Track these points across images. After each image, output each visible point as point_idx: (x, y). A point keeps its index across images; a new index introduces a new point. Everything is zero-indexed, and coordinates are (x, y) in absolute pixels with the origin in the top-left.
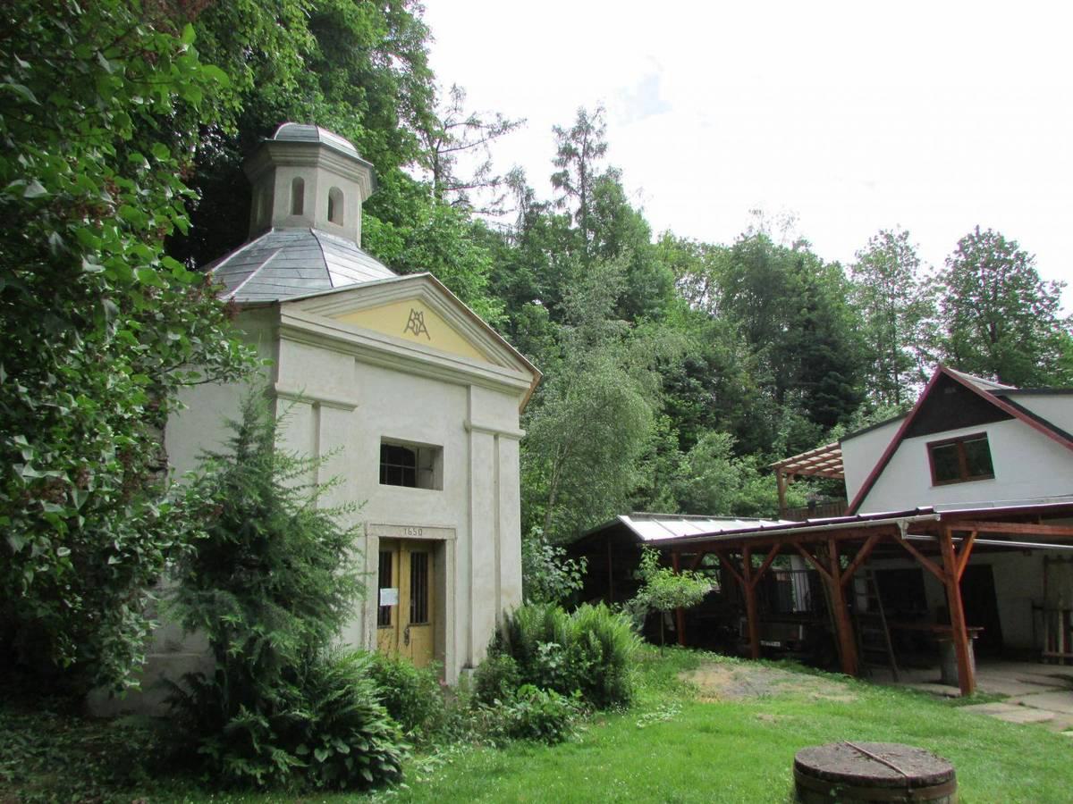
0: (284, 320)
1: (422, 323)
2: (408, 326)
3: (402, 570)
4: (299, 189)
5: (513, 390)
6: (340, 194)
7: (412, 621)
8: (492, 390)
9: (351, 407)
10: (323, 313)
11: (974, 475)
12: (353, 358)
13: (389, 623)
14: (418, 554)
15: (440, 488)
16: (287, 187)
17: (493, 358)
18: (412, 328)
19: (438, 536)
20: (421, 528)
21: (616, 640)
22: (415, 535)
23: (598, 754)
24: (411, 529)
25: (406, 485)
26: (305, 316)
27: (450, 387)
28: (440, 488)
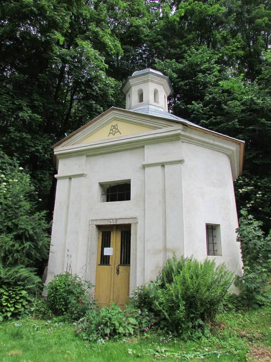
1: (117, 129)
2: (110, 133)
3: (116, 239)
5: (172, 138)
7: (121, 263)
8: (161, 142)
10: (71, 144)
11: (212, 226)
12: (85, 156)
14: (125, 232)
18: (112, 133)
19: (126, 222)
20: (116, 219)
22: (119, 222)
24: (111, 220)
25: (111, 201)
27: (135, 150)
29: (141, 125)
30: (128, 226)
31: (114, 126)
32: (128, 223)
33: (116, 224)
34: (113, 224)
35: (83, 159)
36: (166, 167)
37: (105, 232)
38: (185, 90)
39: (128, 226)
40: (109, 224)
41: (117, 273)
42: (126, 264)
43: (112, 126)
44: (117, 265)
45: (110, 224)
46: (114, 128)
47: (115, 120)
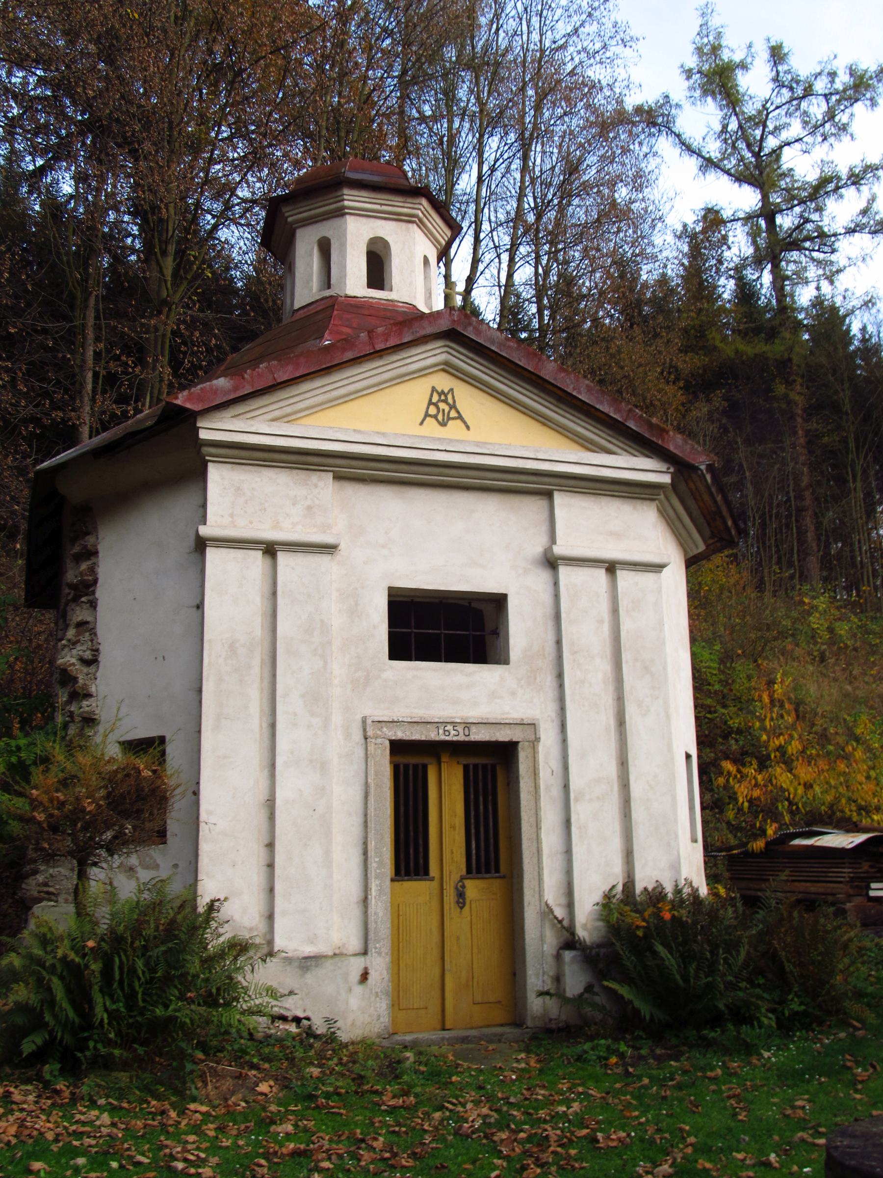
0: (203, 435)
1: (453, 407)
2: (427, 415)
4: (325, 247)
6: (385, 244)
7: (469, 870)
9: (329, 549)
12: (331, 475)
13: (426, 872)
15: (506, 662)
16: (311, 255)
17: (592, 442)
18: (435, 417)
19: (503, 736)
20: (467, 725)
21: (211, 907)
22: (479, 735)
23: (163, 1113)
24: (449, 727)
25: (447, 661)
26: (237, 425)
28: (506, 662)
30: (398, 747)
31: (443, 392)
32: (507, 739)
33: (467, 739)
34: (455, 739)
36: (201, 509)
37: (406, 766)
39: (398, 747)
40: (443, 737)
41: (458, 902)
42: (488, 871)
43: (434, 389)
44: (456, 877)
45: (447, 738)
46: (440, 400)
47: (444, 370)
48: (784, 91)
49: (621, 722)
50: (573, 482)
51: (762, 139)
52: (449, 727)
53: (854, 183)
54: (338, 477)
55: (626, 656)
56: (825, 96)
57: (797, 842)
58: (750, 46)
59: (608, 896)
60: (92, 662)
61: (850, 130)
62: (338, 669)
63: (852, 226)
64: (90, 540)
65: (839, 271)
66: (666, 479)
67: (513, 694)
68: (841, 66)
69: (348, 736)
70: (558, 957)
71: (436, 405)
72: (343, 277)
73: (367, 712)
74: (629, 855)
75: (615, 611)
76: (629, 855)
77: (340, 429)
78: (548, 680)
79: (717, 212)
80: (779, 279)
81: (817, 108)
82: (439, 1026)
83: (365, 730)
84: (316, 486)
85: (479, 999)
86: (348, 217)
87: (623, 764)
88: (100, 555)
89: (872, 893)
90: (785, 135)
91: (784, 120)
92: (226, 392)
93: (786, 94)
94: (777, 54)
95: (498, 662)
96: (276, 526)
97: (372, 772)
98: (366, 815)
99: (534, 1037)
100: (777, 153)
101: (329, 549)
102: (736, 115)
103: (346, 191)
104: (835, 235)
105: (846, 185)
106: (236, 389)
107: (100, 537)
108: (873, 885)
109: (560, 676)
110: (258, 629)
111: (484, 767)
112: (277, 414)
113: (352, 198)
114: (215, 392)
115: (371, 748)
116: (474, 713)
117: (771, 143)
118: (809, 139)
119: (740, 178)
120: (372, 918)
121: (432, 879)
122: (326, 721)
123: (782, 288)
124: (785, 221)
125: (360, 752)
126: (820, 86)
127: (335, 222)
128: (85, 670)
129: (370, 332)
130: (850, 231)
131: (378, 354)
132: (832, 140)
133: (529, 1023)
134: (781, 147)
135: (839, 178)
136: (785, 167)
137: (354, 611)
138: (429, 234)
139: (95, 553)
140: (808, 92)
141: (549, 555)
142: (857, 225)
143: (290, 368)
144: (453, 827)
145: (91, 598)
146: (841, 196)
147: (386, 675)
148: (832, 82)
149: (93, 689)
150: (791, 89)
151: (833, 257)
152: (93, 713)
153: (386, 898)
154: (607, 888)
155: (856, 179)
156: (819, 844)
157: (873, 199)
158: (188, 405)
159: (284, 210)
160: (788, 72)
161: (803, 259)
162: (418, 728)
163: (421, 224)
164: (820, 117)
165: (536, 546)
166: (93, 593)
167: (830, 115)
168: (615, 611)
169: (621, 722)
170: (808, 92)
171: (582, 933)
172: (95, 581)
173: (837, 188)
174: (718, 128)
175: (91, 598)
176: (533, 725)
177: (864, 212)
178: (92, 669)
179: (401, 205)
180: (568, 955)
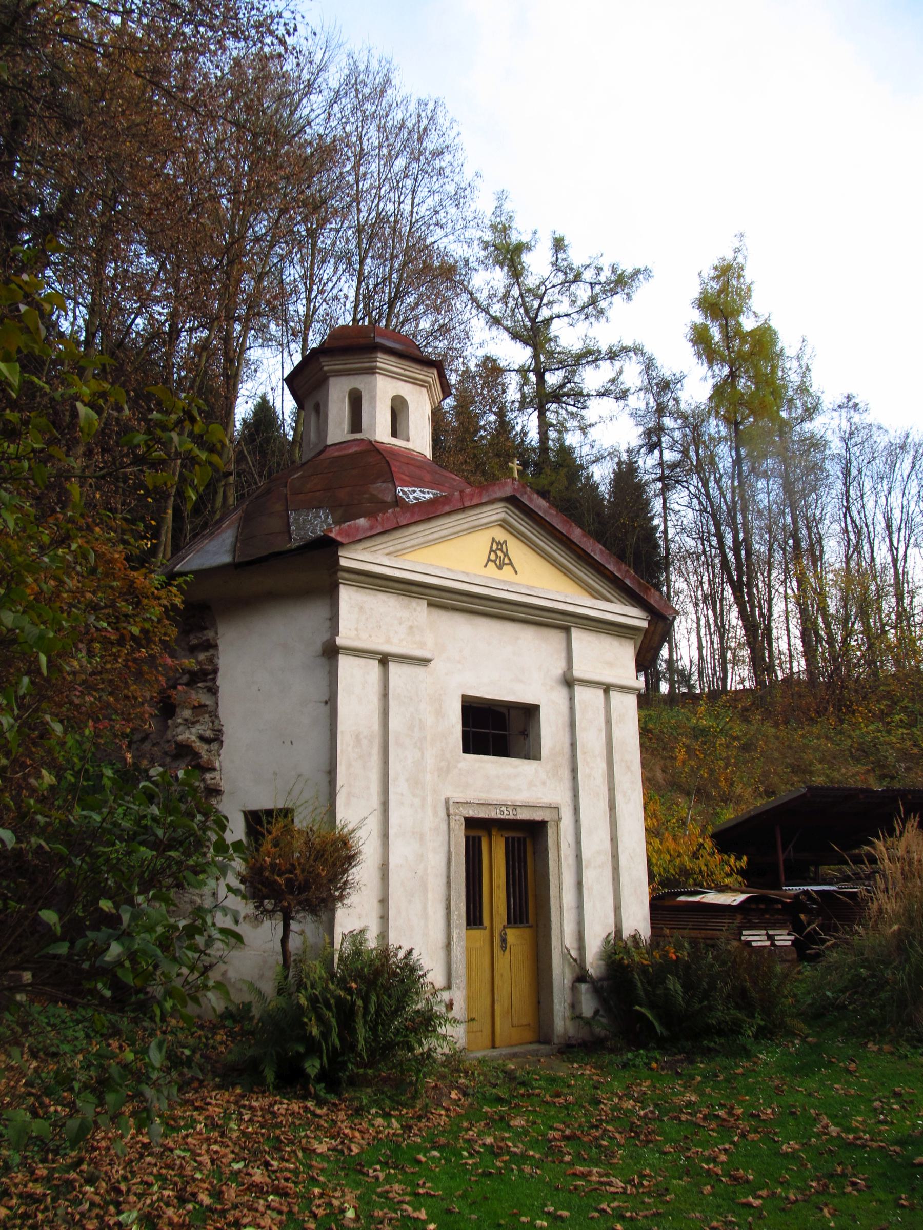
0: (343, 562)
1: (506, 555)
2: (489, 560)
7: (509, 922)
9: (424, 661)
12: (425, 602)
13: (481, 923)
15: (537, 757)
16: (343, 402)
17: (597, 592)
18: (494, 562)
19: (537, 816)
20: (515, 807)
22: (523, 815)
24: (503, 809)
25: (474, 753)
28: (537, 757)
29: (566, 572)
30: (471, 823)
35: (418, 610)
38: (157, 320)
39: (471, 823)
42: (521, 922)
43: (493, 540)
44: (501, 927)
48: (560, 274)
49: (612, 808)
50: (585, 622)
51: (538, 309)
52: (503, 809)
53: (611, 358)
54: (430, 605)
55: (616, 757)
56: (591, 284)
57: (682, 899)
58: (535, 233)
59: (607, 940)
60: (216, 738)
61: (606, 314)
62: (430, 760)
63: (602, 390)
64: (210, 634)
65: (591, 425)
66: (645, 624)
67: (544, 783)
68: (606, 263)
69: (435, 813)
70: (574, 989)
71: (495, 552)
72: (373, 425)
73: (448, 795)
74: (617, 909)
75: (608, 722)
76: (617, 909)
77: (437, 567)
78: (566, 773)
79: (495, 361)
80: (544, 425)
81: (583, 293)
82: (490, 1044)
83: (448, 809)
84: (415, 610)
85: (515, 1022)
86: (379, 378)
87: (614, 839)
88: (220, 648)
89: (743, 938)
90: (556, 309)
91: (557, 297)
92: (365, 530)
93: (561, 276)
94: (559, 245)
95: (527, 757)
96: (388, 641)
97: (452, 843)
98: (448, 877)
99: (561, 1051)
100: (548, 321)
101: (424, 661)
102: (519, 285)
103: (380, 355)
104: (588, 395)
105: (603, 359)
106: (371, 528)
107: (220, 631)
108: (744, 932)
109: (574, 771)
110: (376, 727)
111: (519, 839)
112: (391, 549)
113: (384, 361)
114: (357, 529)
115: (453, 823)
116: (521, 797)
117: (545, 313)
118: (575, 316)
119: (515, 336)
120: (454, 959)
121: (485, 928)
122: (424, 799)
123: (546, 433)
124: (553, 379)
125: (444, 827)
126: (588, 275)
127: (366, 378)
128: (206, 747)
129: (462, 492)
130: (601, 394)
131: (464, 509)
132: (592, 319)
133: (556, 1041)
134: (552, 318)
135: (599, 352)
136: (552, 335)
137: (439, 713)
138: (431, 397)
139: (215, 646)
140: (577, 278)
141: (568, 677)
142: (606, 391)
143: (408, 515)
144: (499, 887)
145: (209, 684)
146: (597, 367)
147: (462, 765)
148: (598, 274)
149: (217, 765)
150: (565, 273)
151: (583, 412)
152: (218, 785)
153: (463, 944)
154: (604, 935)
155: (612, 356)
156: (704, 900)
157: (621, 372)
158: (339, 539)
159: (321, 360)
160: (564, 260)
161: (563, 412)
162: (483, 808)
163: (429, 389)
164: (586, 300)
165: (558, 668)
166: (214, 680)
167: (593, 301)
168: (608, 722)
169: (612, 808)
170: (577, 278)
171: (591, 971)
172: (215, 671)
173: (597, 360)
174: (502, 290)
175: (209, 684)
176: (557, 808)
177: (613, 381)
178: (214, 746)
179: (419, 373)
180: (584, 987)
